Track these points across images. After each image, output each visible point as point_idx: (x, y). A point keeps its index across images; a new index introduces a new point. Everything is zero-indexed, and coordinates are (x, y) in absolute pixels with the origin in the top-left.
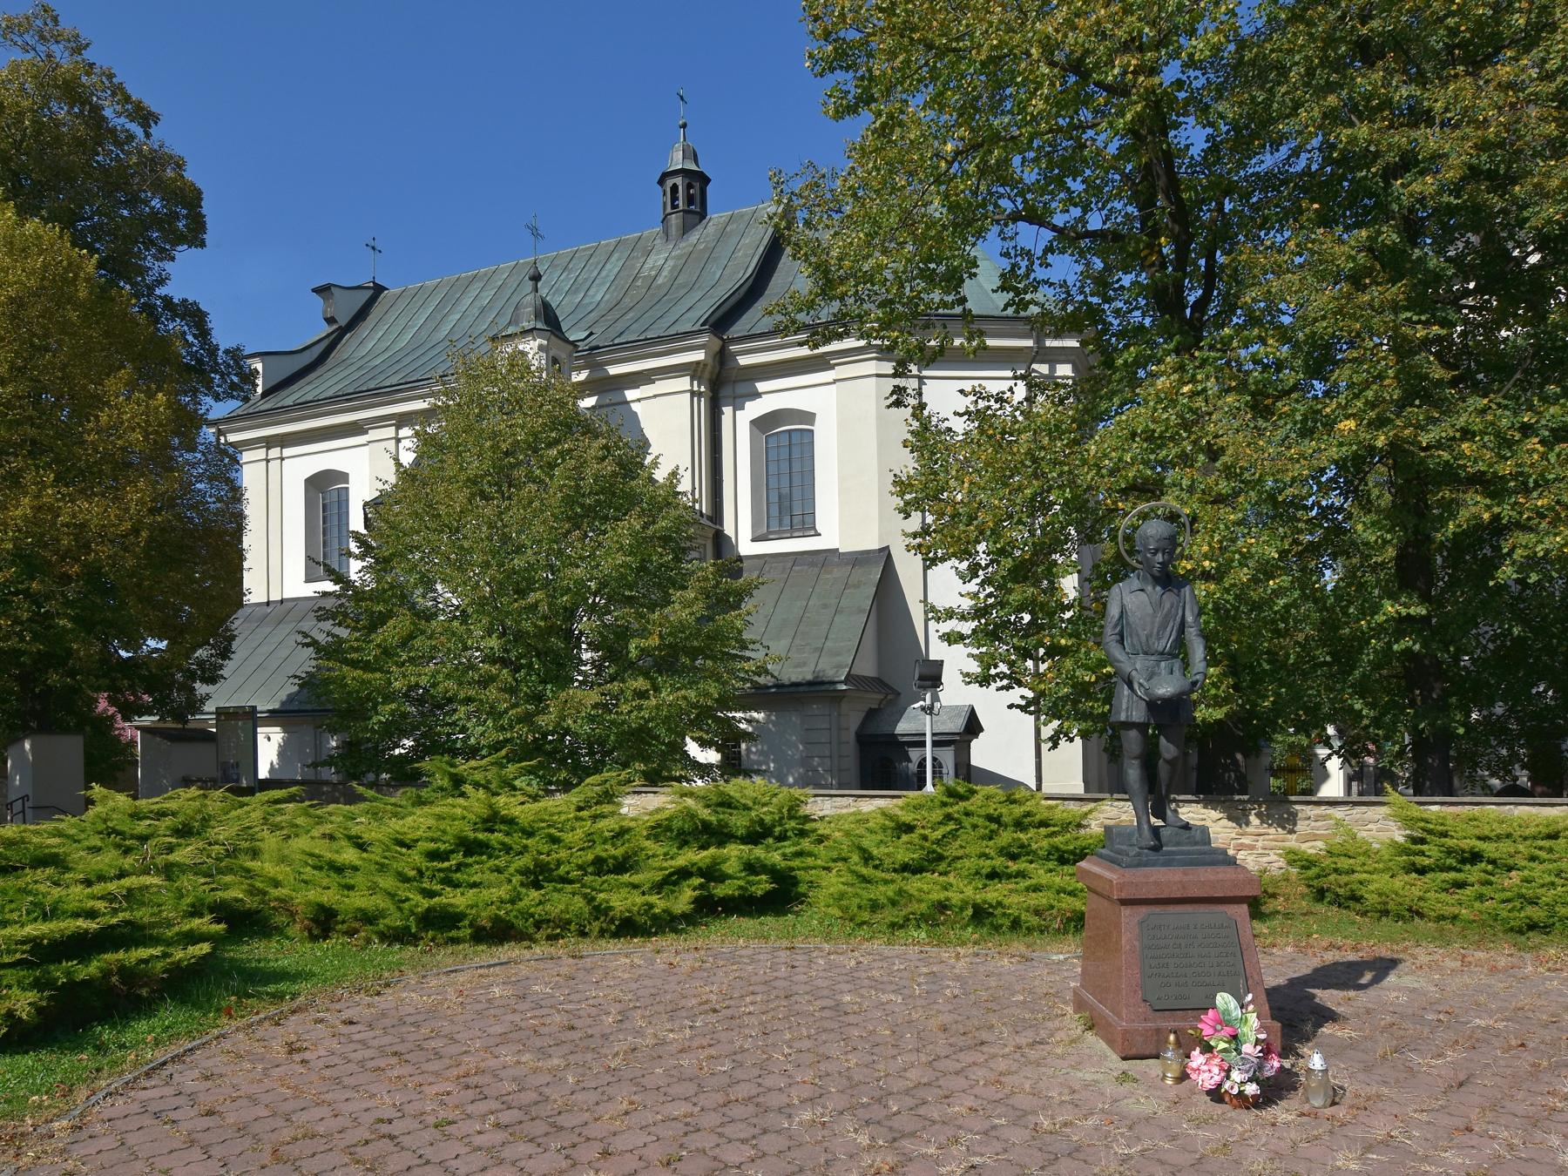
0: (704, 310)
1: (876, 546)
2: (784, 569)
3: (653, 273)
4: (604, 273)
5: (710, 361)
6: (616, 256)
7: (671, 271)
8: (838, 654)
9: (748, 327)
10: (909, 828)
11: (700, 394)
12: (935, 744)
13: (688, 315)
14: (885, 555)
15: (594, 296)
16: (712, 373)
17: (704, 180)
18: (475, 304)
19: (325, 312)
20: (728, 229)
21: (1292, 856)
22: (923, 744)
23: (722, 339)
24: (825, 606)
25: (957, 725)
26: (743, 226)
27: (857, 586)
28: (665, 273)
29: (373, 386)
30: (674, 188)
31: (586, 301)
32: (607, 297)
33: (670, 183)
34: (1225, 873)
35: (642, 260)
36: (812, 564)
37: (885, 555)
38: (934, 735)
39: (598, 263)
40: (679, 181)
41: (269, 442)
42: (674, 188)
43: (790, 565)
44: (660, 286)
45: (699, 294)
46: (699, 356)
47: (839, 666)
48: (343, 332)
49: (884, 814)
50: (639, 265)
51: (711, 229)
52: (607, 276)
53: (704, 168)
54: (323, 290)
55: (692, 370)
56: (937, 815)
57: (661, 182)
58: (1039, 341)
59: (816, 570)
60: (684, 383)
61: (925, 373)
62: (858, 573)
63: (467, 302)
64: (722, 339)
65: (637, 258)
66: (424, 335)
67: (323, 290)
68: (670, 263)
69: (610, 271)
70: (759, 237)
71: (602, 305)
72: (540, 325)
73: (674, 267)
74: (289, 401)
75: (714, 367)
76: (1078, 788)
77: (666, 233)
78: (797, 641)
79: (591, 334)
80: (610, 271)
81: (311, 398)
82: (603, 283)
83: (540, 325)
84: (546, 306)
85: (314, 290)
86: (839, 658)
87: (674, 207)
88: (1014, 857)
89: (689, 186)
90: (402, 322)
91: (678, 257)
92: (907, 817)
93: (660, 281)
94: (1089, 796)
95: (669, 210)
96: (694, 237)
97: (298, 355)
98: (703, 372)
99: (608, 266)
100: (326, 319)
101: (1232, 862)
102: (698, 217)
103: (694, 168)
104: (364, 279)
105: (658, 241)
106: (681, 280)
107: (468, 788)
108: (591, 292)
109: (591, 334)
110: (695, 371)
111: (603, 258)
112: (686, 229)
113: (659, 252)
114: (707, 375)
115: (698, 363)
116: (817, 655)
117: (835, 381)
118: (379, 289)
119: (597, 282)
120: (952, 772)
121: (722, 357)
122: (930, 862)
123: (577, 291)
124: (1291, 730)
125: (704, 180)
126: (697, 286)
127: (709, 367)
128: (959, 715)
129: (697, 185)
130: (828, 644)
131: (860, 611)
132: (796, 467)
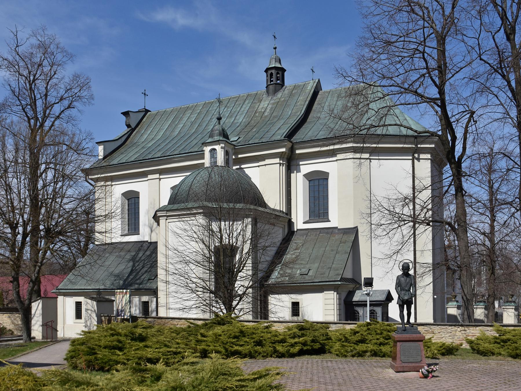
0: (285, 130)
1: (352, 226)
2: (316, 234)
3: (263, 110)
4: (242, 109)
5: (287, 152)
6: (247, 101)
7: (271, 110)
8: (337, 270)
9: (302, 137)
10: (358, 332)
11: (283, 164)
12: (370, 305)
13: (279, 132)
14: (355, 230)
15: (238, 119)
16: (288, 156)
17: (283, 70)
18: (189, 120)
19: (126, 122)
20: (293, 92)
21: (468, 341)
22: (366, 305)
23: (291, 142)
24: (332, 250)
25: (383, 298)
26: (299, 91)
27: (345, 243)
28: (268, 111)
29: (150, 157)
30: (271, 74)
31: (236, 121)
32: (244, 121)
33: (270, 72)
34: (418, 335)
35: (258, 104)
36: (327, 233)
37: (355, 230)
38: (370, 301)
39: (240, 104)
40: (273, 71)
41: (106, 179)
42: (271, 74)
43: (318, 233)
44: (266, 117)
45: (283, 121)
46: (284, 150)
47: (338, 275)
48: (133, 130)
49: (351, 329)
50: (257, 106)
51: (286, 92)
52: (244, 111)
53: (284, 65)
54: (126, 114)
55: (280, 156)
56: (365, 328)
57: (266, 71)
58: (416, 145)
59: (329, 235)
60: (277, 160)
61: (371, 158)
62: (345, 237)
63: (185, 119)
64: (291, 142)
65: (256, 103)
66: (168, 133)
67: (126, 114)
68: (270, 106)
69: (245, 108)
70: (306, 97)
71: (242, 124)
72: (221, 138)
73: (272, 108)
74: (115, 162)
75: (288, 154)
76: (431, 321)
77: (268, 92)
78: (321, 264)
79: (239, 138)
80: (245, 108)
81: (124, 161)
82: (242, 114)
83: (221, 138)
84: (223, 130)
85: (122, 113)
86: (338, 272)
87: (271, 81)
88: (387, 339)
89: (278, 73)
90: (158, 127)
91: (273, 104)
92: (358, 330)
93: (266, 114)
94: (435, 324)
95: (269, 83)
96: (279, 95)
97: (116, 142)
98: (284, 155)
99: (244, 106)
100: (127, 125)
101: (420, 333)
102: (281, 86)
103: (279, 66)
104: (141, 107)
105: (264, 96)
106: (274, 114)
107: (28, 374)
108: (237, 118)
109: (239, 138)
110: (281, 155)
111: (242, 102)
112: (276, 91)
113: (265, 101)
114: (286, 156)
115: (283, 152)
116: (329, 270)
117: (337, 160)
118: (147, 111)
119: (240, 113)
120: (381, 316)
121: (292, 150)
122: (363, 341)
123: (231, 117)
124: (435, 297)
125: (283, 70)
126: (281, 118)
127: (287, 154)
128: (384, 293)
129: (280, 72)
130: (334, 266)
131: (346, 253)
132: (321, 194)
